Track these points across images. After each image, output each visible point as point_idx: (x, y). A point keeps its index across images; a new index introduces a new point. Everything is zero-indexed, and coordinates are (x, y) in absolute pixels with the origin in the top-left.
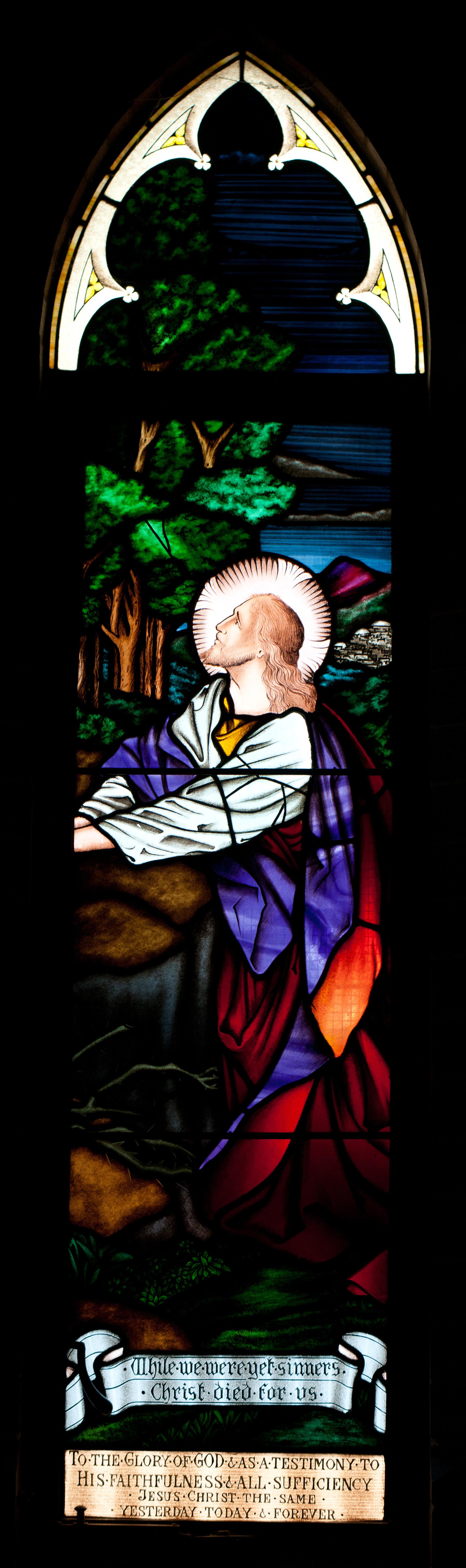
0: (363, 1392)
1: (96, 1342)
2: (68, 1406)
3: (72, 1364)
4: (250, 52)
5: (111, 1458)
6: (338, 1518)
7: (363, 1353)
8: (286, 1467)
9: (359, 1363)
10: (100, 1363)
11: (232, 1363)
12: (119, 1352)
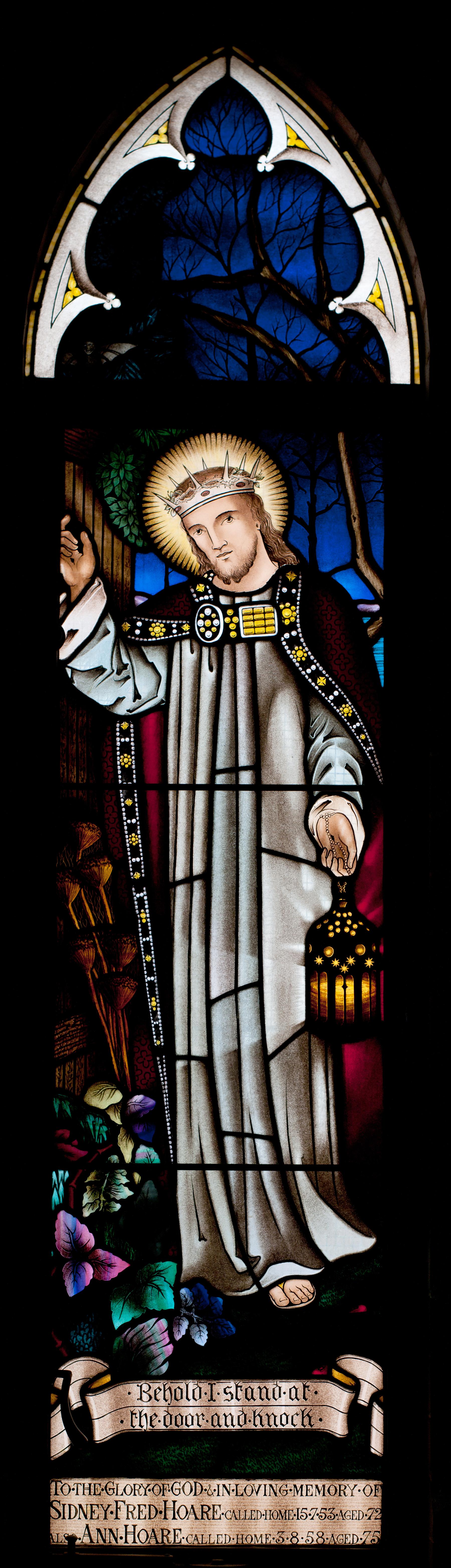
0: (358, 1416)
1: (79, 1369)
2: (53, 1433)
3: (56, 1391)
4: (237, 47)
5: (304, 1488)
6: (222, 1541)
7: (359, 1376)
8: (309, 1494)
9: (355, 1386)
10: (87, 1389)
11: (262, 1387)
12: (107, 1379)
